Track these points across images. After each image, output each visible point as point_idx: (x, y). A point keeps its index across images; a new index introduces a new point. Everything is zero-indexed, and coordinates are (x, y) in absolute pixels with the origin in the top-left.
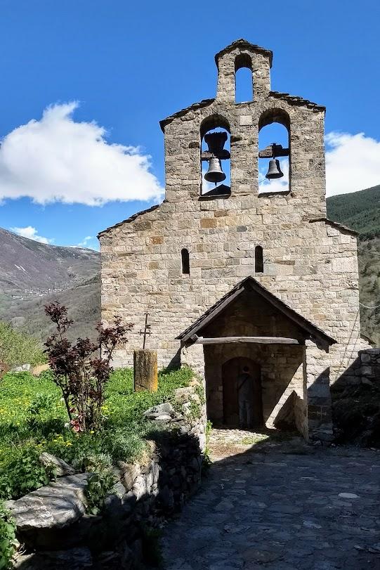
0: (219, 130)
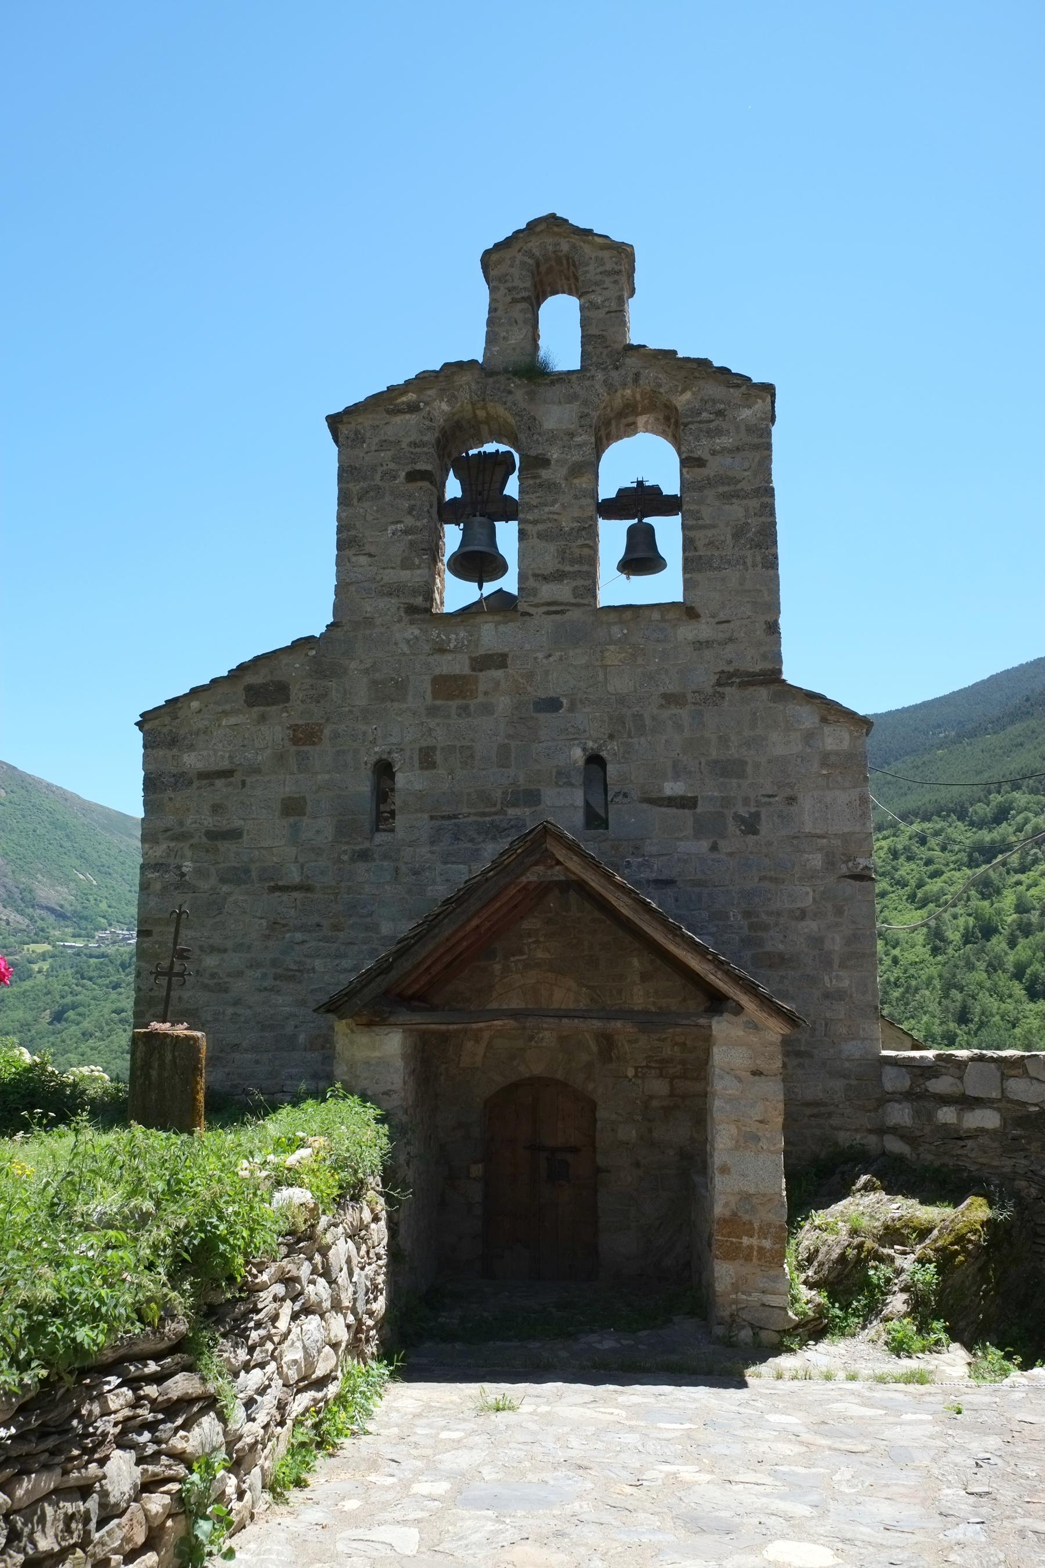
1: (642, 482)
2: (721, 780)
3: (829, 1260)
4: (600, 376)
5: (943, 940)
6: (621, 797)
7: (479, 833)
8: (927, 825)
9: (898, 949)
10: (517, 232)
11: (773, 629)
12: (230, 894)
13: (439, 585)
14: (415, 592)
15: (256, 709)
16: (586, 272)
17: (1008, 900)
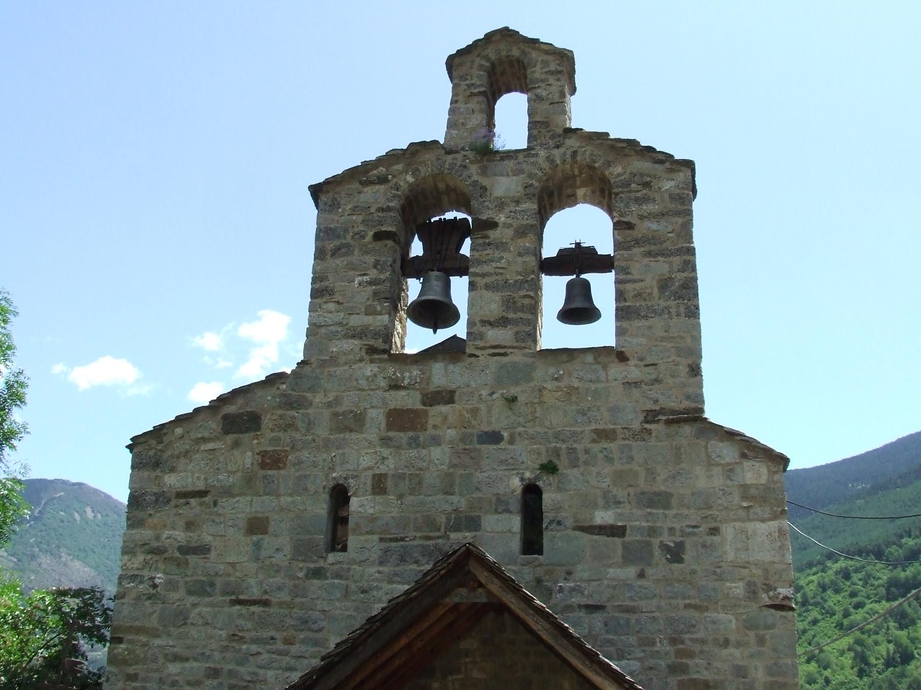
1: (580, 243)
2: (649, 510)
4: (542, 153)
6: (555, 524)
7: (423, 556)
9: (829, 670)
10: (476, 42)
11: (695, 371)
12: (194, 605)
13: (400, 330)
14: (376, 335)
16: (534, 72)
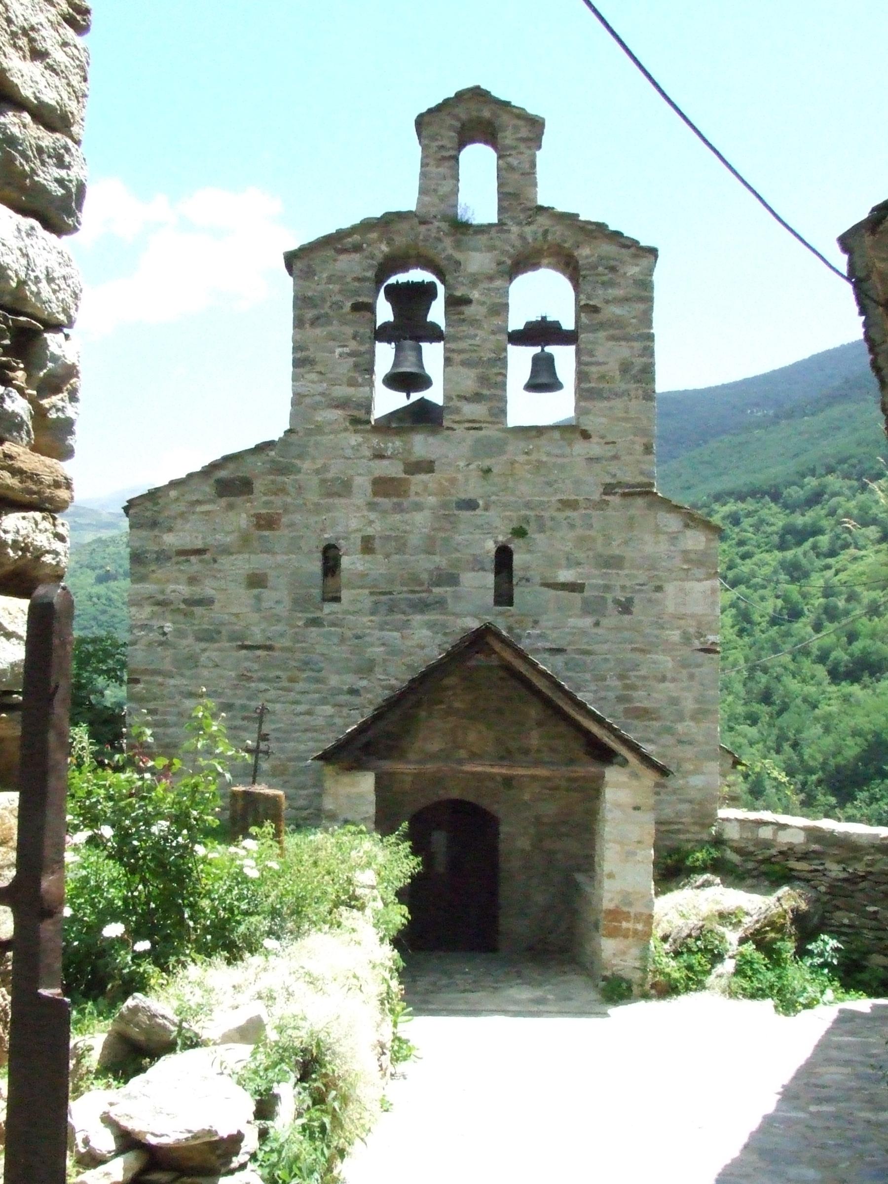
0: (417, 275)
3: (680, 937)
5: (749, 621)
6: (524, 581)
8: (741, 505)
15: (224, 499)
17: (817, 581)
